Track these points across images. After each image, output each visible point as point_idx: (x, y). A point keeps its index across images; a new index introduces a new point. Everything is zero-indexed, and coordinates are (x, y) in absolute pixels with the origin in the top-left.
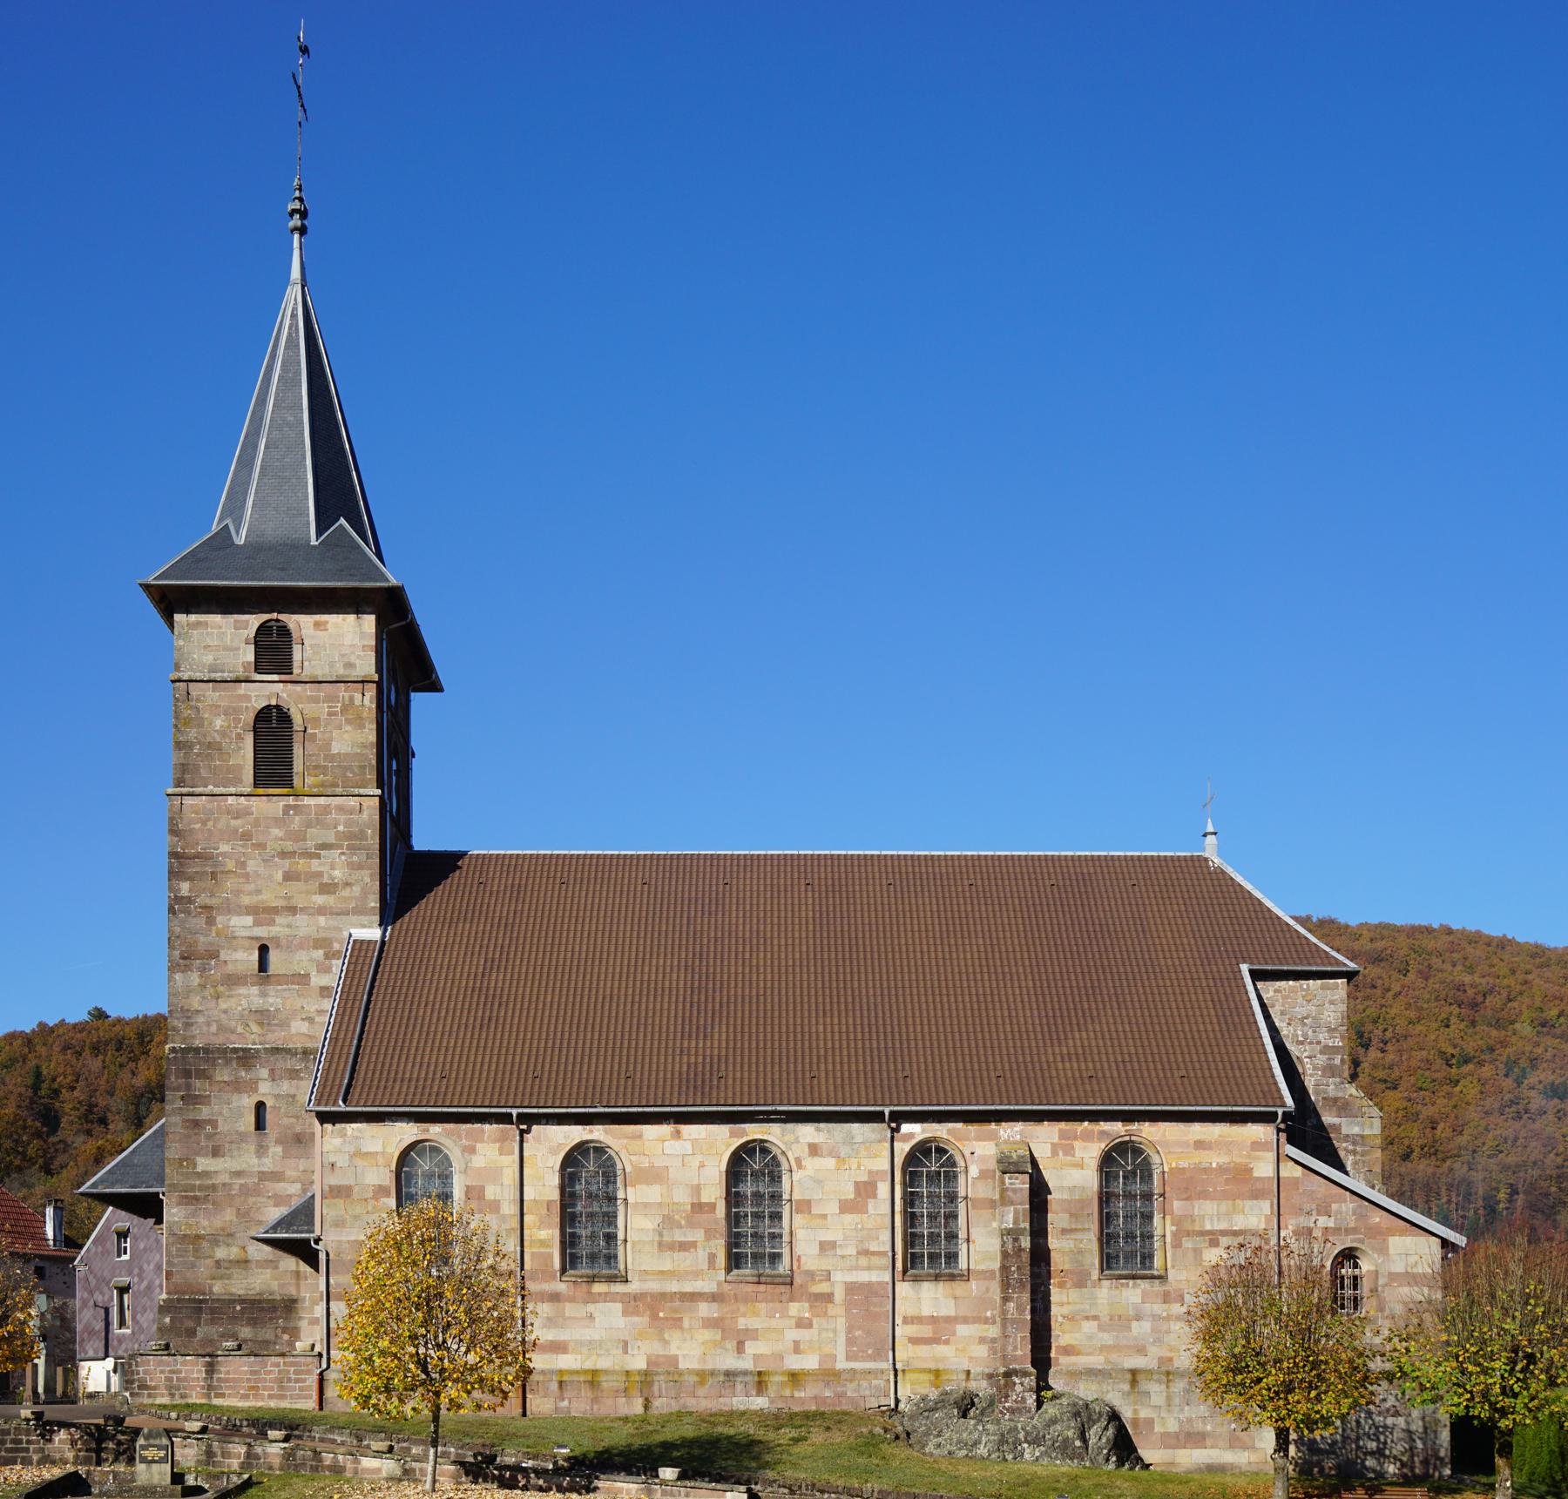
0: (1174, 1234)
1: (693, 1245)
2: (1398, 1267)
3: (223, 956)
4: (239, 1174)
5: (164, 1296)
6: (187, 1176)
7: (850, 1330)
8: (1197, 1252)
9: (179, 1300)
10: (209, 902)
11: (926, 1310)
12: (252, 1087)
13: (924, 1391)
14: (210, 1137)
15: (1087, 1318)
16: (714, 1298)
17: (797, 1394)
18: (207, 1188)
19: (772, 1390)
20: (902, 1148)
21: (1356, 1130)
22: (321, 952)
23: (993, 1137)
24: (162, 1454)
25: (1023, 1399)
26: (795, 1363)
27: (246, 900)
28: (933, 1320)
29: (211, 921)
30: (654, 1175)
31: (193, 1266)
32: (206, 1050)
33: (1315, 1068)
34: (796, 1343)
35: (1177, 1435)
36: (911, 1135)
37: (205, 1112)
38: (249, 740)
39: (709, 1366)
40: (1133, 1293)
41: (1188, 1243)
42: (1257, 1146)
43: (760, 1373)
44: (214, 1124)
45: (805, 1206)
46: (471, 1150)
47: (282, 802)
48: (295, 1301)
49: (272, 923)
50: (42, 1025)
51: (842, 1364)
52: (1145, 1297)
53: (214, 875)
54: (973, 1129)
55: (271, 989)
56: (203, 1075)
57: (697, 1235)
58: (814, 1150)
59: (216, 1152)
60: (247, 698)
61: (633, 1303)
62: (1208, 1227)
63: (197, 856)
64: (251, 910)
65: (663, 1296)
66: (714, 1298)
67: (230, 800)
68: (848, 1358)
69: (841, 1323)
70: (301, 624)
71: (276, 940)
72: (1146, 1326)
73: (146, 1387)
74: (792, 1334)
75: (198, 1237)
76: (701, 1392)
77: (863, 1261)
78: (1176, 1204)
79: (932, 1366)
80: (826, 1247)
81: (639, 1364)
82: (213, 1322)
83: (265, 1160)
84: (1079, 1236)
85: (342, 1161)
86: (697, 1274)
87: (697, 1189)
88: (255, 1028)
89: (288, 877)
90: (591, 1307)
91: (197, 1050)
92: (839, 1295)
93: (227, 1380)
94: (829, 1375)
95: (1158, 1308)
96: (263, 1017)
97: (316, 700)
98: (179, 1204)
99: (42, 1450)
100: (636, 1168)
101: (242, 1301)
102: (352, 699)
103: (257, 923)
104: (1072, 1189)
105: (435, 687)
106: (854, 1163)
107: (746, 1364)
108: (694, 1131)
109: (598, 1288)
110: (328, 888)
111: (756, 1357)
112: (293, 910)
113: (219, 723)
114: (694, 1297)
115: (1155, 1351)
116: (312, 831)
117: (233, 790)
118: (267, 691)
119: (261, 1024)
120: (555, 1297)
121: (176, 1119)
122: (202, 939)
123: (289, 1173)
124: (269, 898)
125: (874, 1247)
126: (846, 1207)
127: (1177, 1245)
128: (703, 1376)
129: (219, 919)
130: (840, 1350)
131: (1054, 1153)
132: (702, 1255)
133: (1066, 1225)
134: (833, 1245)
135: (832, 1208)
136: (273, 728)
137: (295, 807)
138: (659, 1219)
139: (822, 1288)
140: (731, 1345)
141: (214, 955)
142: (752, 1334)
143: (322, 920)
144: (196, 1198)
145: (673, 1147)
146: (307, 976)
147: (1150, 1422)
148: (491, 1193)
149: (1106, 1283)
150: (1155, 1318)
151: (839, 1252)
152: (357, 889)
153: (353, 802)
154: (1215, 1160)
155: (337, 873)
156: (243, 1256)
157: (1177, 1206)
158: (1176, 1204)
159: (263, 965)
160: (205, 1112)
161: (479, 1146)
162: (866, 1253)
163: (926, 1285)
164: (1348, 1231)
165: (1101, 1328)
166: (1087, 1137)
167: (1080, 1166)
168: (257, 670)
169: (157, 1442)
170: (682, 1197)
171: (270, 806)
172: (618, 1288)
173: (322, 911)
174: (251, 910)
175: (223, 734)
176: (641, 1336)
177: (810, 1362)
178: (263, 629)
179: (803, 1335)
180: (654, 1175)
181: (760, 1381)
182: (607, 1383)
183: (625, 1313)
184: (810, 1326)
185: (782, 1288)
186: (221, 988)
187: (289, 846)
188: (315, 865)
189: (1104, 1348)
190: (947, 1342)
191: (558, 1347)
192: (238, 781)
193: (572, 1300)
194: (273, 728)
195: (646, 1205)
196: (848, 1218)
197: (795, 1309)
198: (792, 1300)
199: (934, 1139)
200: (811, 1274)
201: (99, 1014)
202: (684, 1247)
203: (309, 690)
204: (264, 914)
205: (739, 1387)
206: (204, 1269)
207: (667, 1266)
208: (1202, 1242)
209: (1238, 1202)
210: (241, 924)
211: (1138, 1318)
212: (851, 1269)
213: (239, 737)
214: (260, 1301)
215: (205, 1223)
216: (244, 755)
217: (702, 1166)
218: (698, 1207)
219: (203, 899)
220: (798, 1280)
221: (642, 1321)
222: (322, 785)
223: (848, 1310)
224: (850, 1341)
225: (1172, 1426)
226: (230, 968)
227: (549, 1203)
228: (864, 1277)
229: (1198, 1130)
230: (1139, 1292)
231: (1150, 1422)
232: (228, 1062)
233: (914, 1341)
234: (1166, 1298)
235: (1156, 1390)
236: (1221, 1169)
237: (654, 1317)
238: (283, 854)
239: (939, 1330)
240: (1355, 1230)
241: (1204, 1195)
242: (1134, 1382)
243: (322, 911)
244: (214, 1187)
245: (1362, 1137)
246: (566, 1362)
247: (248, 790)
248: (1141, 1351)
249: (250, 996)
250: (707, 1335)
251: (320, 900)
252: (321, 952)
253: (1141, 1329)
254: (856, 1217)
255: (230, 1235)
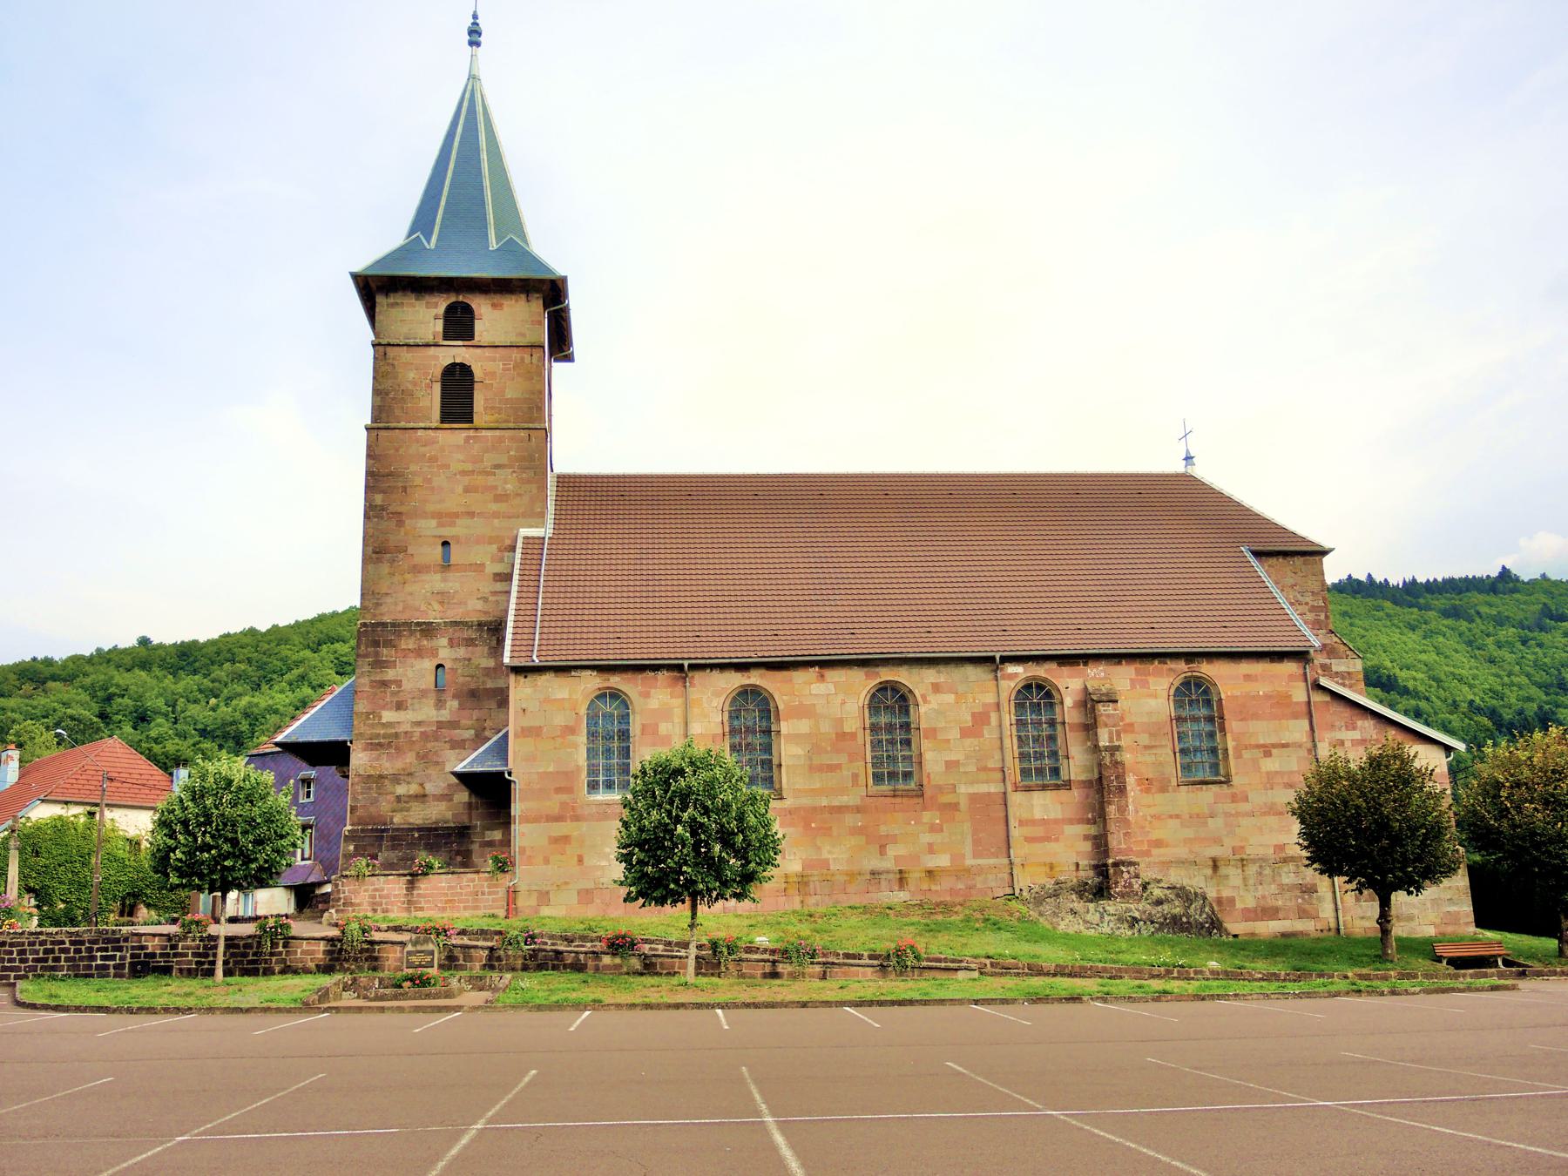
0: (1235, 748)
1: (839, 767)
3: (410, 551)
4: (419, 723)
5: (349, 827)
6: (372, 726)
8: (1255, 761)
9: (363, 831)
10: (400, 509)
11: (1038, 814)
12: (434, 652)
14: (394, 694)
15: (1171, 817)
16: (858, 810)
17: (934, 888)
18: (390, 736)
19: (912, 885)
21: (1343, 669)
22: (495, 547)
24: (429, 958)
25: (1131, 885)
27: (430, 508)
28: (1044, 822)
29: (400, 523)
30: (803, 712)
31: (376, 800)
32: (394, 625)
35: (1255, 910)
37: (390, 674)
38: (437, 388)
40: (1208, 795)
41: (1247, 755)
42: (1291, 677)
43: (901, 872)
44: (399, 683)
45: (932, 733)
46: (646, 695)
47: (465, 434)
48: (468, 828)
49: (453, 524)
50: (99, 650)
53: (405, 489)
54: (1066, 670)
55: (451, 575)
56: (389, 644)
57: (842, 759)
58: (936, 688)
59: (400, 706)
63: (390, 474)
64: (438, 515)
66: (858, 810)
67: (420, 433)
68: (976, 855)
70: (482, 306)
73: (352, 904)
74: (926, 838)
75: (381, 777)
76: (851, 888)
77: (983, 776)
78: (1234, 724)
79: (1048, 861)
80: (951, 765)
82: (393, 848)
83: (443, 712)
84: (1158, 751)
85: (532, 706)
86: (842, 791)
87: (840, 721)
88: (436, 606)
89: (467, 490)
91: (384, 625)
92: (964, 804)
93: (424, 896)
95: (1231, 808)
96: (443, 597)
98: (365, 750)
99: (284, 961)
101: (419, 830)
102: (522, 359)
103: (440, 525)
104: (1150, 714)
110: (499, 498)
112: (471, 514)
113: (411, 375)
114: (840, 809)
115: (1229, 843)
117: (422, 425)
118: (457, 353)
119: (442, 603)
121: (365, 680)
122: (392, 537)
123: (464, 722)
125: (991, 765)
127: (1239, 756)
130: (968, 849)
131: (1133, 686)
133: (1147, 742)
134: (957, 763)
135: (954, 734)
136: (458, 383)
139: (946, 799)
142: (893, 839)
144: (380, 745)
145: (818, 688)
146: (483, 565)
147: (1232, 901)
148: (663, 728)
150: (1227, 815)
152: (526, 499)
156: (421, 791)
158: (1234, 724)
159: (446, 557)
160: (390, 674)
161: (653, 691)
162: (985, 769)
163: (1036, 794)
166: (1158, 674)
168: (445, 338)
169: (424, 948)
170: (826, 727)
171: (455, 437)
173: (496, 515)
177: (942, 861)
178: (450, 309)
179: (936, 838)
180: (803, 712)
185: (916, 800)
186: (408, 576)
188: (491, 481)
189: (1187, 841)
190: (1057, 840)
194: (458, 383)
195: (798, 736)
196: (968, 741)
197: (927, 816)
198: (925, 809)
199: (1034, 678)
200: (940, 788)
201: (144, 642)
202: (832, 768)
203: (488, 352)
205: (883, 883)
206: (385, 806)
208: (1258, 753)
210: (428, 527)
212: (972, 783)
214: (436, 829)
215: (387, 765)
216: (432, 400)
217: (843, 703)
218: (842, 736)
219: (394, 508)
220: (928, 792)
224: (976, 842)
225: (1250, 903)
226: (416, 560)
228: (983, 788)
229: (1246, 667)
231: (1232, 901)
232: (412, 633)
234: (1234, 798)
235: (1233, 874)
236: (1267, 697)
237: (807, 826)
239: (1047, 831)
241: (1255, 716)
242: (1215, 867)
243: (496, 515)
244: (396, 735)
247: (434, 425)
248: (1218, 841)
249: (435, 581)
251: (494, 507)
252: (495, 547)
253: (1216, 824)
254: (975, 741)
255: (410, 774)
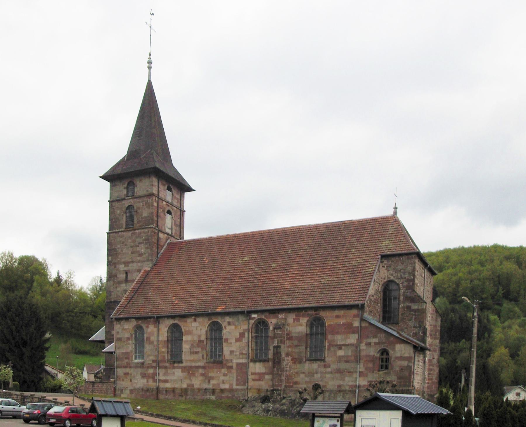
0: (328, 346)
2: (398, 355)
7: (237, 376)
8: (335, 352)
11: (257, 371)
13: (255, 395)
15: (302, 373)
20: (252, 322)
21: (416, 307)
23: (277, 317)
26: (223, 386)
27: (123, 260)
28: (259, 374)
29: (115, 267)
33: (403, 287)
34: (223, 381)
36: (255, 318)
39: (201, 387)
40: (315, 366)
45: (226, 340)
46: (148, 327)
51: (235, 387)
52: (319, 366)
55: (128, 284)
57: (199, 349)
58: (229, 323)
60: (124, 204)
61: (184, 369)
62: (339, 343)
64: (124, 263)
65: (191, 367)
68: (237, 385)
69: (235, 375)
71: (129, 271)
72: (319, 375)
74: (222, 378)
77: (241, 356)
79: (258, 387)
80: (232, 352)
81: (185, 386)
86: (199, 361)
87: (200, 336)
90: (174, 370)
92: (234, 366)
94: (231, 390)
95: (323, 370)
97: (139, 202)
100: (186, 331)
103: (125, 266)
105: (190, 189)
106: (239, 327)
107: (211, 387)
108: (199, 320)
109: (176, 365)
110: (141, 255)
111: (213, 385)
112: (133, 262)
114: (198, 367)
116: (138, 239)
120: (166, 367)
124: (127, 259)
125: (244, 352)
126: (237, 340)
128: (199, 390)
129: (117, 266)
130: (234, 384)
131: (294, 321)
132: (200, 355)
135: (233, 341)
137: (134, 233)
138: (190, 345)
139: (230, 364)
140: (207, 381)
141: (116, 276)
142: (212, 378)
143: (139, 264)
149: (307, 362)
150: (321, 373)
151: (235, 354)
152: (147, 254)
153: (146, 230)
154: (342, 321)
155: (143, 250)
157: (329, 337)
164: (383, 343)
165: (305, 376)
166: (303, 316)
167: (301, 325)
170: (196, 338)
172: (180, 365)
173: (139, 262)
174: (124, 263)
175: (119, 215)
176: (186, 378)
177: (227, 386)
179: (226, 378)
180: (189, 333)
181: (213, 392)
182: (177, 391)
183: (182, 372)
184: (227, 375)
187: (132, 244)
190: (262, 380)
191: (166, 381)
192: (122, 227)
193: (170, 368)
195: (187, 341)
196: (238, 344)
197: (224, 370)
198: (223, 368)
200: (227, 360)
202: (196, 353)
204: (127, 264)
207: (192, 359)
209: (349, 335)
210: (122, 267)
211: (317, 373)
213: (123, 215)
217: (201, 329)
218: (200, 341)
220: (224, 362)
221: (185, 374)
222: (140, 226)
223: (237, 371)
224: (237, 380)
226: (119, 280)
227: (165, 341)
230: (317, 364)
233: (254, 380)
234: (325, 366)
236: (344, 324)
238: (131, 247)
240: (385, 343)
241: (338, 333)
243: (139, 262)
245: (418, 309)
246: (168, 385)
250: (201, 378)
251: (139, 258)
